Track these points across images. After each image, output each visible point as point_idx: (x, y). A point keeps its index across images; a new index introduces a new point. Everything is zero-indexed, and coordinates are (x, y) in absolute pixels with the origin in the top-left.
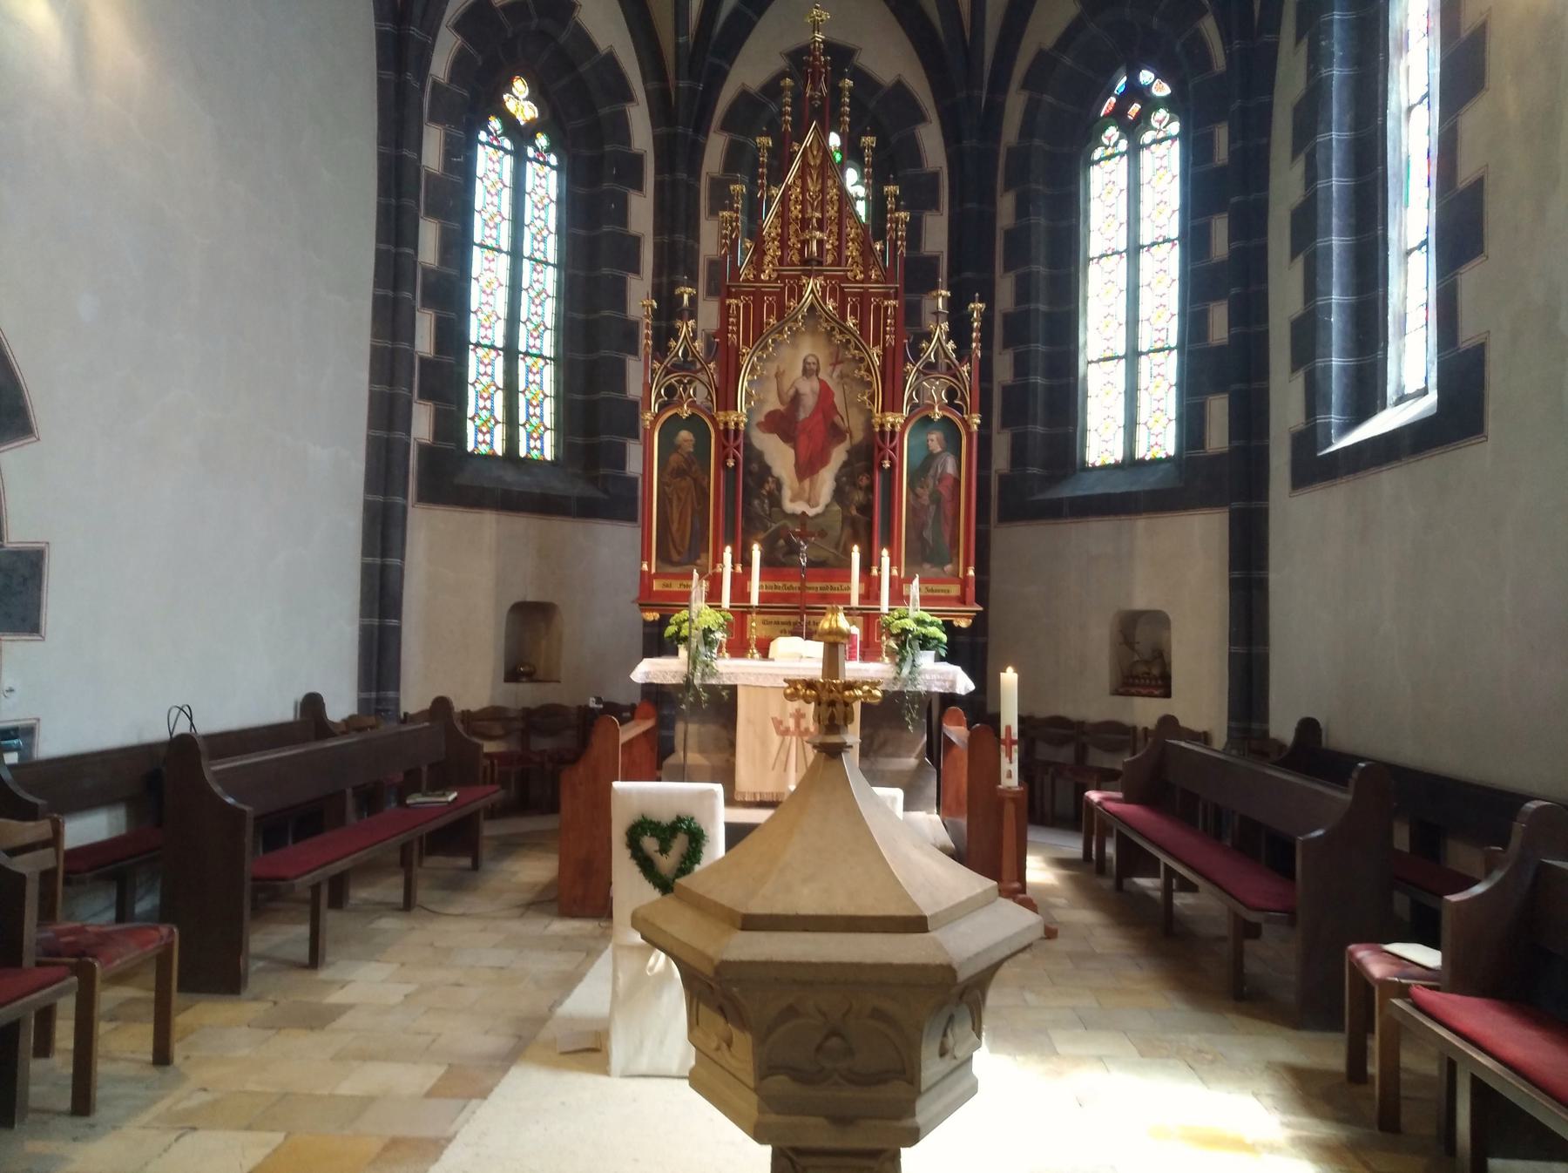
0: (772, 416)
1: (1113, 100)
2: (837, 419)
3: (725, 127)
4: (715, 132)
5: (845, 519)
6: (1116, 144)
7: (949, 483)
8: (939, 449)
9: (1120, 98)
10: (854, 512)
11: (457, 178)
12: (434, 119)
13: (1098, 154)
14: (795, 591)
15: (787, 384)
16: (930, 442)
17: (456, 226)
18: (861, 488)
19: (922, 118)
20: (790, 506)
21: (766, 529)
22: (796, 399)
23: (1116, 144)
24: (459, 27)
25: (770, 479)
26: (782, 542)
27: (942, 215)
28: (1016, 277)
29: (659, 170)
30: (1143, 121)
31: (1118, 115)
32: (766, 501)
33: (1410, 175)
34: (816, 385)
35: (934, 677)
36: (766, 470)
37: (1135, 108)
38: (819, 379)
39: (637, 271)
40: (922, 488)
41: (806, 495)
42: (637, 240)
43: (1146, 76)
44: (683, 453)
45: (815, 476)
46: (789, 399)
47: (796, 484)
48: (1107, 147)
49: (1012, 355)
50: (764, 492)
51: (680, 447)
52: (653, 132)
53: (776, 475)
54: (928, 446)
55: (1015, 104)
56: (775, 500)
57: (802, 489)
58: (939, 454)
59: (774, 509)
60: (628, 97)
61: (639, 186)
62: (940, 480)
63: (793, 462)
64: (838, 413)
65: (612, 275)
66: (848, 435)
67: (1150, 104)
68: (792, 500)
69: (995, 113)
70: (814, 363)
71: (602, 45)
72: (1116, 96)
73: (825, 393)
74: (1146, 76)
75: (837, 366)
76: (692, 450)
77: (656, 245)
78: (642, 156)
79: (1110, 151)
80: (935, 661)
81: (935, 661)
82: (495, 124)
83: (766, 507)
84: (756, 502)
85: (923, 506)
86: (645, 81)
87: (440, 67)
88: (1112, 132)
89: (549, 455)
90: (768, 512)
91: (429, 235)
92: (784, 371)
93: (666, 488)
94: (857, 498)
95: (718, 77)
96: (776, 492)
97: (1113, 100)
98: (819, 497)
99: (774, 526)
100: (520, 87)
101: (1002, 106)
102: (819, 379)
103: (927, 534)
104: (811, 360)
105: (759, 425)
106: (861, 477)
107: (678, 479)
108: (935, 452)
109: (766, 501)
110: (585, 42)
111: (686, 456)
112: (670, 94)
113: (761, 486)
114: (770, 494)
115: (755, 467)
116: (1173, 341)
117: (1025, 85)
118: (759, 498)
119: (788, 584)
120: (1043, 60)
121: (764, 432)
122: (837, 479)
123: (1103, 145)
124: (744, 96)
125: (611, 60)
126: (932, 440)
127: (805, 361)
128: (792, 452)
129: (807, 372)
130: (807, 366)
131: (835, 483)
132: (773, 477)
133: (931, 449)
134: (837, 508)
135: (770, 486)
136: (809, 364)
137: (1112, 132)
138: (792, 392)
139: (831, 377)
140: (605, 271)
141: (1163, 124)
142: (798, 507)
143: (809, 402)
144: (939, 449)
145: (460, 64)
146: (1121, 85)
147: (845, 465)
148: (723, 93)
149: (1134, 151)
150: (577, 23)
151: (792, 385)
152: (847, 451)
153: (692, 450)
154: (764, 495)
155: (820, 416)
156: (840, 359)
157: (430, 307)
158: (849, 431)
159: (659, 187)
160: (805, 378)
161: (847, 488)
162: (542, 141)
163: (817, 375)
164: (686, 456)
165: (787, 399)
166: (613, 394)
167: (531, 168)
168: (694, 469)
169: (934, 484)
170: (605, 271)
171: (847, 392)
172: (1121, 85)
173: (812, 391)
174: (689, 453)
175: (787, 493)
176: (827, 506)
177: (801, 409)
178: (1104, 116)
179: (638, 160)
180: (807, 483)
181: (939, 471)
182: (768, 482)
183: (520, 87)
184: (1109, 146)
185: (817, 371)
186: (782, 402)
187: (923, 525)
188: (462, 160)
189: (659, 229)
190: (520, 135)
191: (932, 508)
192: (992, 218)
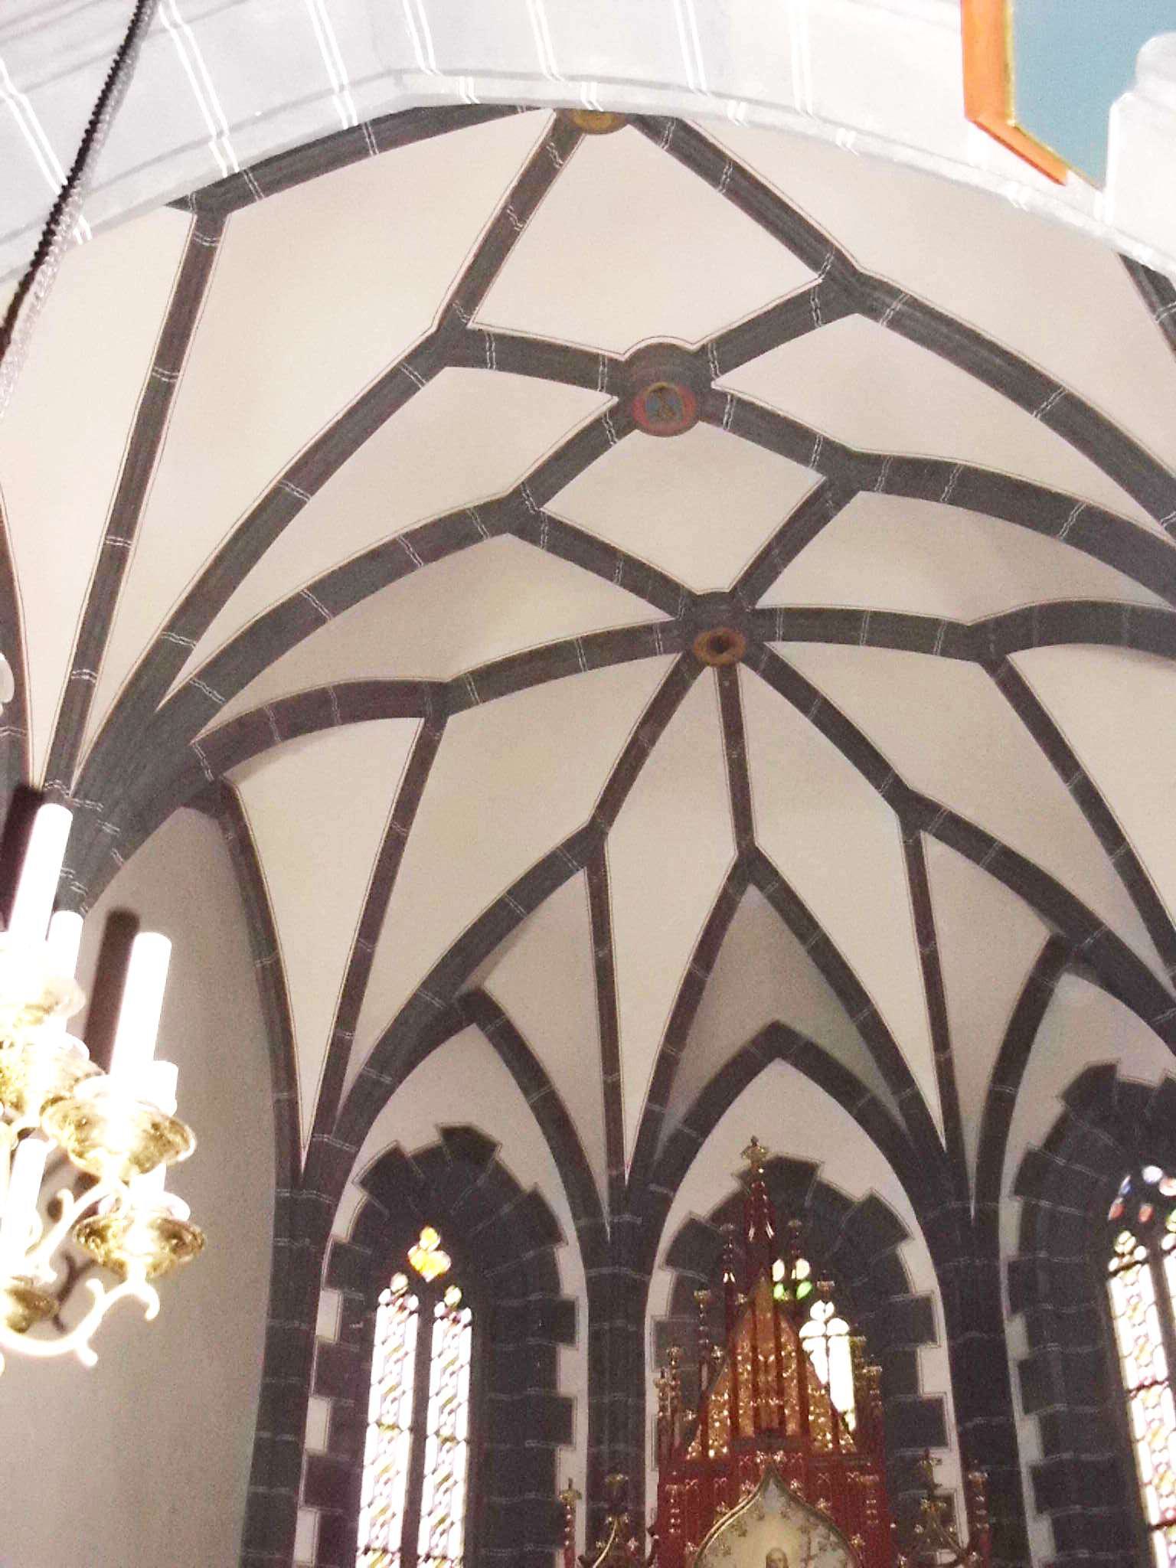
1: (1119, 1201)
6: (1131, 1253)
9: (1127, 1199)
11: (355, 1348)
12: (333, 1283)
13: (1114, 1264)
17: (350, 1402)
19: (903, 1235)
23: (1131, 1253)
24: (364, 1183)
27: (940, 1346)
28: (1041, 1421)
29: (593, 1318)
31: (1128, 1221)
35: (485, 1382)
37: (1146, 1212)
43: (1152, 1174)
49: (1050, 1521)
52: (587, 1273)
55: (1010, 1212)
60: (553, 1234)
61: (569, 1338)
69: (989, 1221)
71: (526, 1181)
74: (1152, 1174)
78: (574, 1303)
79: (1126, 1260)
80: (155, 1060)
81: (155, 1060)
82: (399, 1282)
86: (576, 1217)
87: (342, 1226)
88: (1125, 1241)
91: (318, 1415)
97: (1119, 1201)
100: (430, 1237)
101: (995, 1213)
110: (505, 1181)
116: (1158, 1537)
117: (1019, 1189)
120: (1034, 1168)
123: (1116, 1254)
124: (692, 1228)
125: (535, 1200)
128: (861, 492)
137: (1125, 1241)
145: (365, 1219)
146: (1125, 1185)
148: (665, 1229)
149: (1156, 1259)
150: (497, 1163)
157: (313, 1504)
159: (595, 1337)
162: (453, 1295)
167: (439, 1327)
172: (1125, 1185)
183: (430, 1237)
188: (361, 1325)
189: (596, 1386)
190: (428, 1292)
192: (1000, 1348)
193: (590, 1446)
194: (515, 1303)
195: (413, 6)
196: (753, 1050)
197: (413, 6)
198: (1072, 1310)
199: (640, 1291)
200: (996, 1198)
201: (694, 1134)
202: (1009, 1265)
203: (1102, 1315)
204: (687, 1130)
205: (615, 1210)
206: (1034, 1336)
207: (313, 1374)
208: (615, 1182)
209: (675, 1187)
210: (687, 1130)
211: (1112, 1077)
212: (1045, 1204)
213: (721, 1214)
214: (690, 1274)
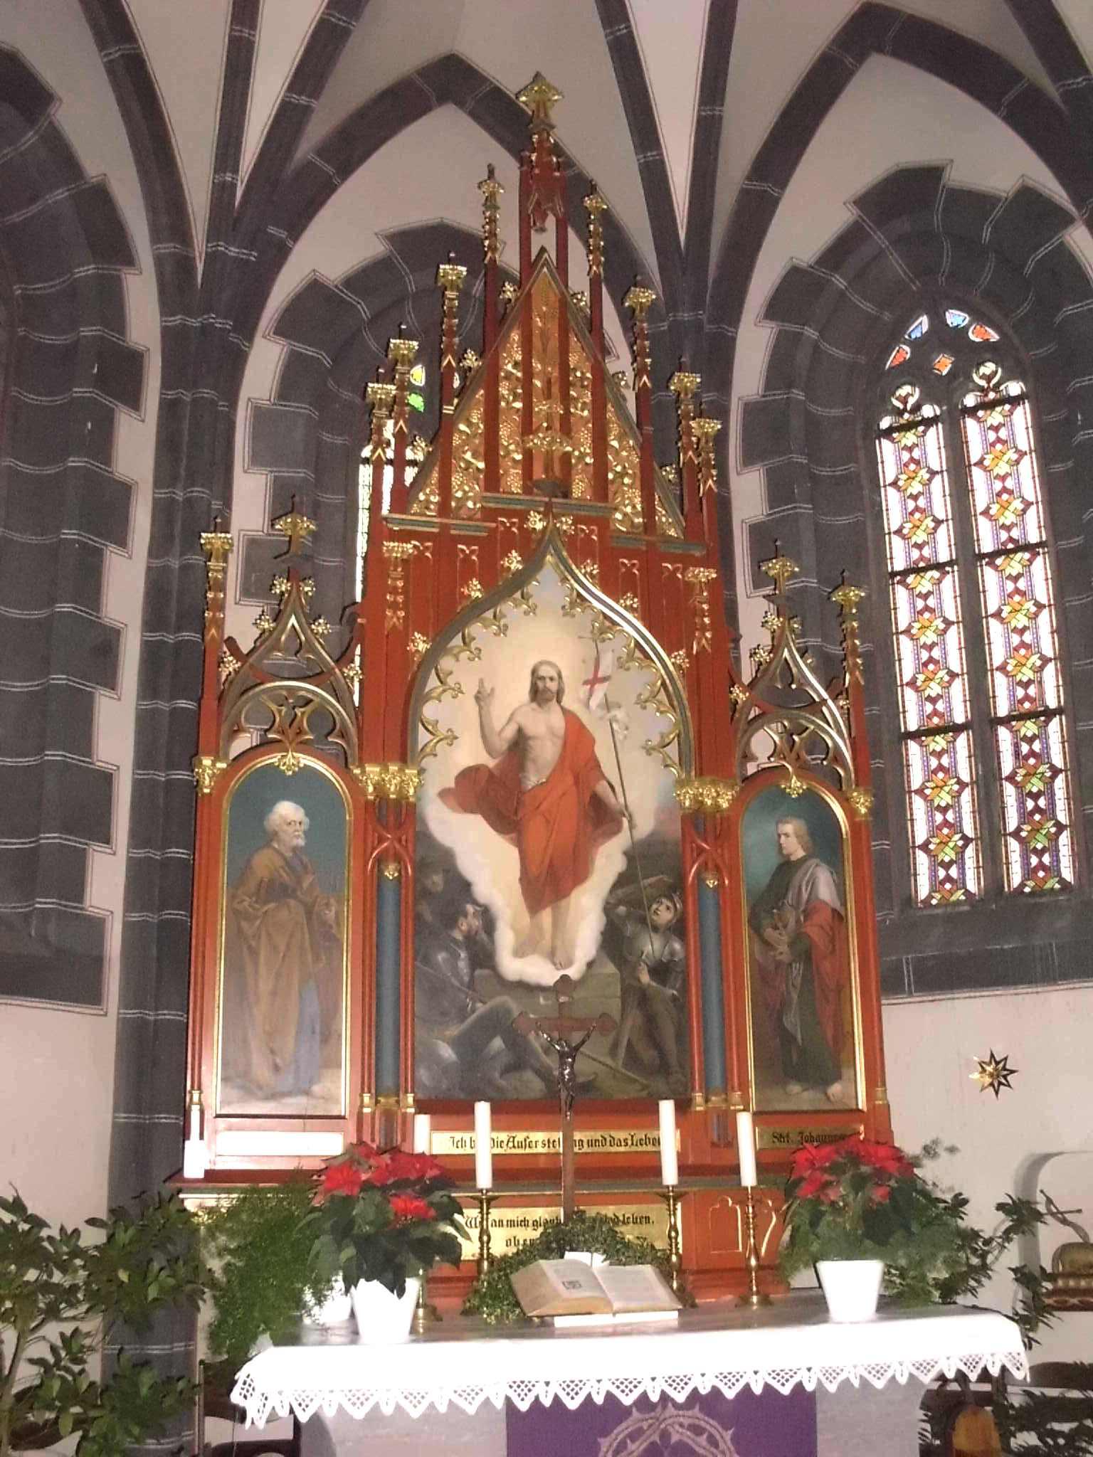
0: (468, 775)
2: (602, 788)
3: (284, 328)
4: (264, 337)
5: (626, 991)
7: (823, 918)
8: (800, 853)
10: (645, 978)
14: (534, 1151)
15: (499, 715)
16: (783, 838)
18: (655, 929)
20: (512, 966)
21: (463, 1014)
22: (520, 745)
23: (917, 408)
25: (470, 908)
26: (497, 1043)
30: (960, 377)
31: (917, 371)
32: (463, 955)
33: (480, 740)
34: (558, 721)
36: (464, 888)
38: (562, 708)
39: (122, 542)
40: (776, 928)
41: (546, 942)
42: (125, 491)
44: (283, 850)
45: (563, 903)
46: (505, 746)
47: (526, 918)
48: (900, 413)
50: (458, 936)
51: (275, 835)
53: (482, 900)
54: (780, 847)
56: (483, 956)
57: (537, 927)
58: (802, 861)
59: (478, 972)
62: (807, 914)
63: (518, 874)
64: (604, 777)
65: (78, 541)
66: (625, 821)
67: (969, 355)
68: (519, 952)
70: (552, 679)
72: (912, 344)
73: (577, 737)
75: (597, 686)
76: (301, 842)
77: (156, 502)
83: (463, 965)
84: (441, 957)
85: (778, 964)
89: (945, 373)
90: (466, 979)
92: (493, 690)
93: (244, 924)
94: (648, 948)
95: (278, 255)
96: (484, 936)
98: (573, 946)
99: (481, 1008)
102: (562, 708)
103: (792, 1021)
104: (545, 671)
105: (444, 794)
106: (655, 906)
107: (272, 905)
108: (793, 858)
109: (463, 955)
111: (289, 854)
112: (194, 268)
113: (451, 922)
114: (470, 939)
115: (437, 881)
117: (775, 309)
118: (447, 949)
119: (520, 1136)
121: (454, 810)
122: (608, 909)
124: (314, 289)
126: (787, 835)
127: (534, 672)
128: (514, 853)
129: (538, 694)
130: (540, 684)
131: (604, 919)
132: (475, 903)
133: (785, 852)
134: (610, 968)
135: (470, 922)
136: (543, 678)
138: (510, 732)
139: (587, 705)
140: (69, 534)
141: (994, 381)
142: (540, 971)
143: (546, 752)
144: (800, 853)
147: (622, 880)
149: (953, 420)
151: (510, 720)
152: (626, 853)
153: (301, 842)
154: (455, 941)
155: (570, 780)
156: (600, 675)
158: (625, 811)
159: (169, 409)
160: (534, 705)
161: (629, 929)
163: (559, 701)
164: (289, 854)
165: (502, 744)
166: (73, 758)
168: (305, 885)
169: (798, 921)
170: (69, 534)
171: (619, 737)
173: (552, 732)
174: (295, 849)
175: (505, 939)
176: (590, 965)
177: (530, 766)
178: (891, 368)
179: (135, 360)
180: (546, 916)
181: (805, 896)
182: (466, 916)
184: (905, 410)
185: (559, 695)
186: (490, 751)
187: (785, 1004)
191: (798, 969)
193: (152, 554)
194: (59, 340)
195: (3, 685)
196: (419, 81)
197: (3, 685)
198: (825, 472)
199: (235, 362)
200: (735, 320)
201: (330, 169)
202: (746, 405)
203: (865, 482)
204: (319, 162)
205: (214, 233)
206: (778, 492)
207: (696, 1051)
208: (221, 192)
209: (295, 233)
210: (319, 162)
211: (940, 178)
212: (811, 333)
213: (361, 280)
214: (310, 351)
